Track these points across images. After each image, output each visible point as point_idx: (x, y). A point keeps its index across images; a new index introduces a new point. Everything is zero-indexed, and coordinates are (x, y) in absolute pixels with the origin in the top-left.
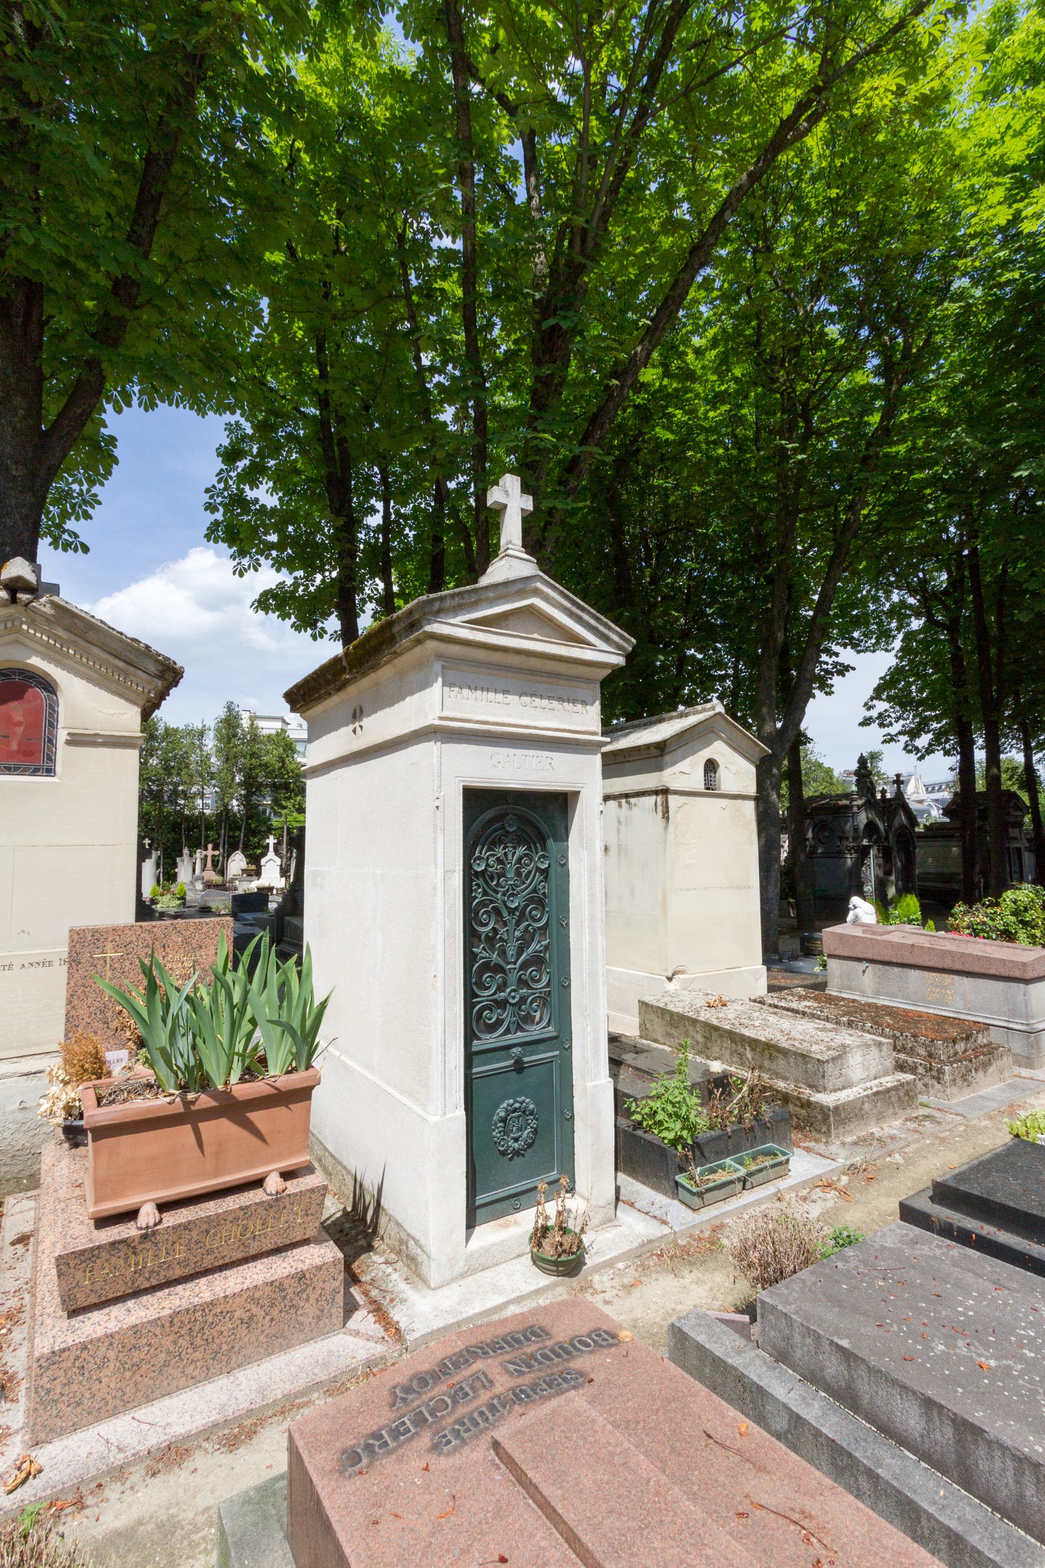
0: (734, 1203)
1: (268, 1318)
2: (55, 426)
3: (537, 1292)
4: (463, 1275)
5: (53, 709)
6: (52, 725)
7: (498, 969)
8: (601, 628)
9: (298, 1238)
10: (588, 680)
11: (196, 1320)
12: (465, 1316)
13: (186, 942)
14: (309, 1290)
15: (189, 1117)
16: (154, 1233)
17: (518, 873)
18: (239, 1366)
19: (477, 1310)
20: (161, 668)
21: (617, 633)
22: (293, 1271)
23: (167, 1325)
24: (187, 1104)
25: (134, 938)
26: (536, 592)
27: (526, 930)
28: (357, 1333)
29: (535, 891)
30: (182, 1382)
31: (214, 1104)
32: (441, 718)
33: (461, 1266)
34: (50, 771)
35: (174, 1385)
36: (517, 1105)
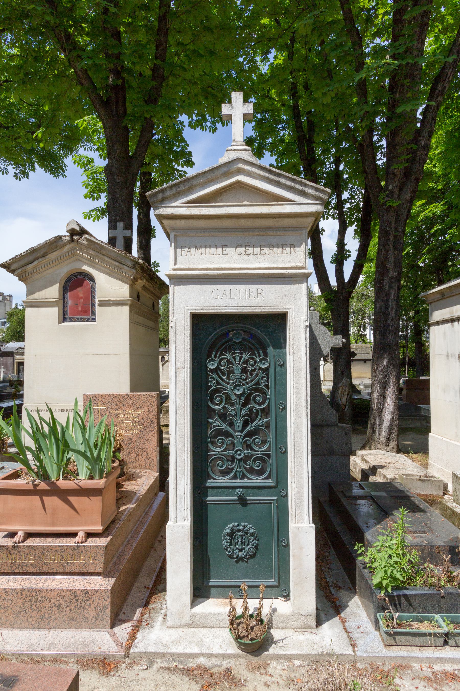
0: (430, 653)
1: (68, 608)
2: (135, 154)
3: (224, 656)
4: (188, 626)
5: (94, 289)
6: (94, 297)
7: (228, 435)
8: (297, 186)
9: (92, 571)
10: (295, 228)
11: (32, 596)
12: (169, 651)
13: (134, 404)
14: (91, 601)
15: (41, 493)
16: (18, 546)
17: (244, 370)
18: (54, 628)
19: (178, 651)
20: (133, 263)
21: (313, 188)
22: (82, 588)
23: (19, 594)
24: (35, 486)
25: (110, 401)
26: (240, 171)
27: (251, 410)
28: (113, 635)
29: (258, 383)
30: (27, 624)
31: (48, 488)
32: (174, 270)
33: (186, 619)
34: (94, 320)
35: (23, 624)
36: (241, 527)
